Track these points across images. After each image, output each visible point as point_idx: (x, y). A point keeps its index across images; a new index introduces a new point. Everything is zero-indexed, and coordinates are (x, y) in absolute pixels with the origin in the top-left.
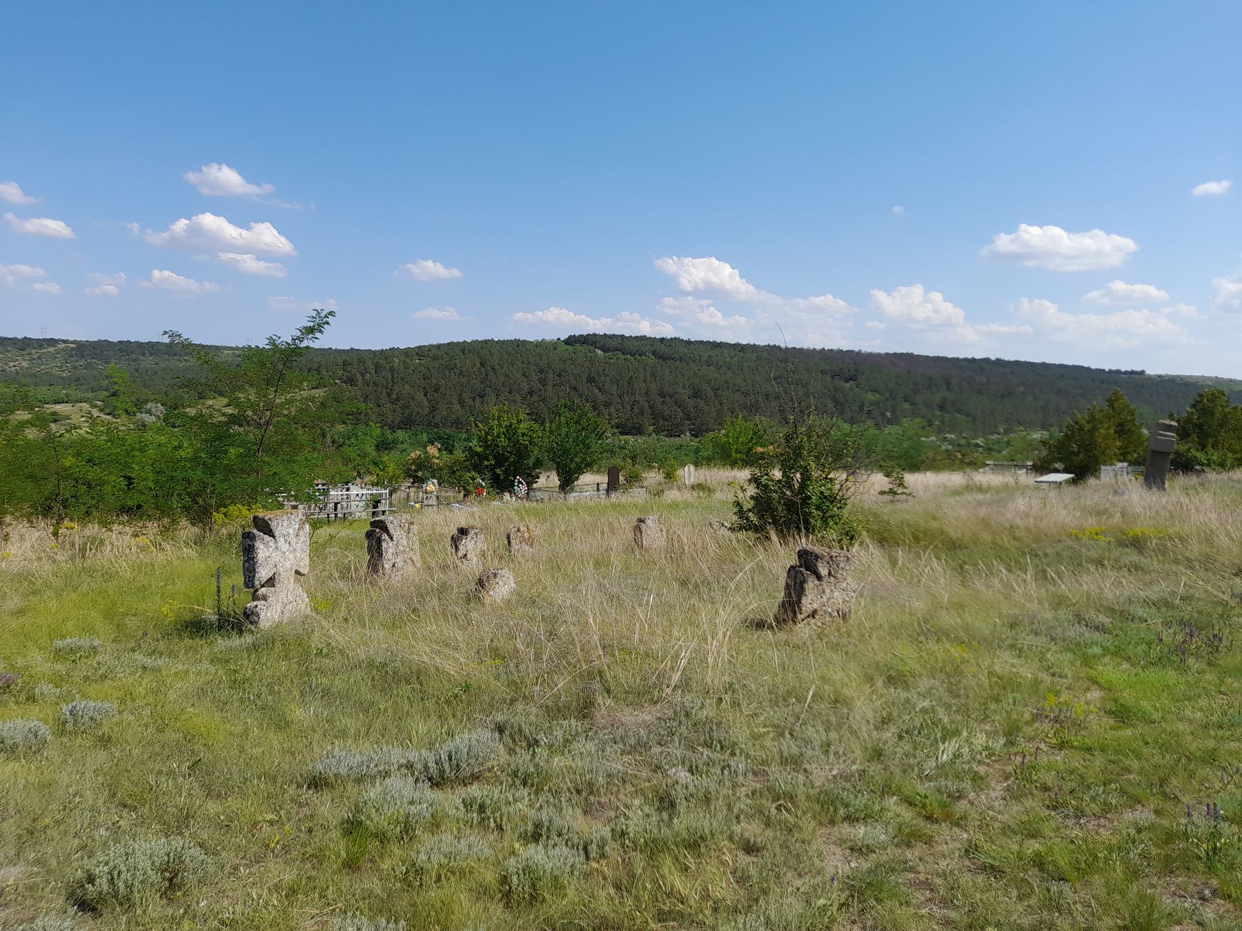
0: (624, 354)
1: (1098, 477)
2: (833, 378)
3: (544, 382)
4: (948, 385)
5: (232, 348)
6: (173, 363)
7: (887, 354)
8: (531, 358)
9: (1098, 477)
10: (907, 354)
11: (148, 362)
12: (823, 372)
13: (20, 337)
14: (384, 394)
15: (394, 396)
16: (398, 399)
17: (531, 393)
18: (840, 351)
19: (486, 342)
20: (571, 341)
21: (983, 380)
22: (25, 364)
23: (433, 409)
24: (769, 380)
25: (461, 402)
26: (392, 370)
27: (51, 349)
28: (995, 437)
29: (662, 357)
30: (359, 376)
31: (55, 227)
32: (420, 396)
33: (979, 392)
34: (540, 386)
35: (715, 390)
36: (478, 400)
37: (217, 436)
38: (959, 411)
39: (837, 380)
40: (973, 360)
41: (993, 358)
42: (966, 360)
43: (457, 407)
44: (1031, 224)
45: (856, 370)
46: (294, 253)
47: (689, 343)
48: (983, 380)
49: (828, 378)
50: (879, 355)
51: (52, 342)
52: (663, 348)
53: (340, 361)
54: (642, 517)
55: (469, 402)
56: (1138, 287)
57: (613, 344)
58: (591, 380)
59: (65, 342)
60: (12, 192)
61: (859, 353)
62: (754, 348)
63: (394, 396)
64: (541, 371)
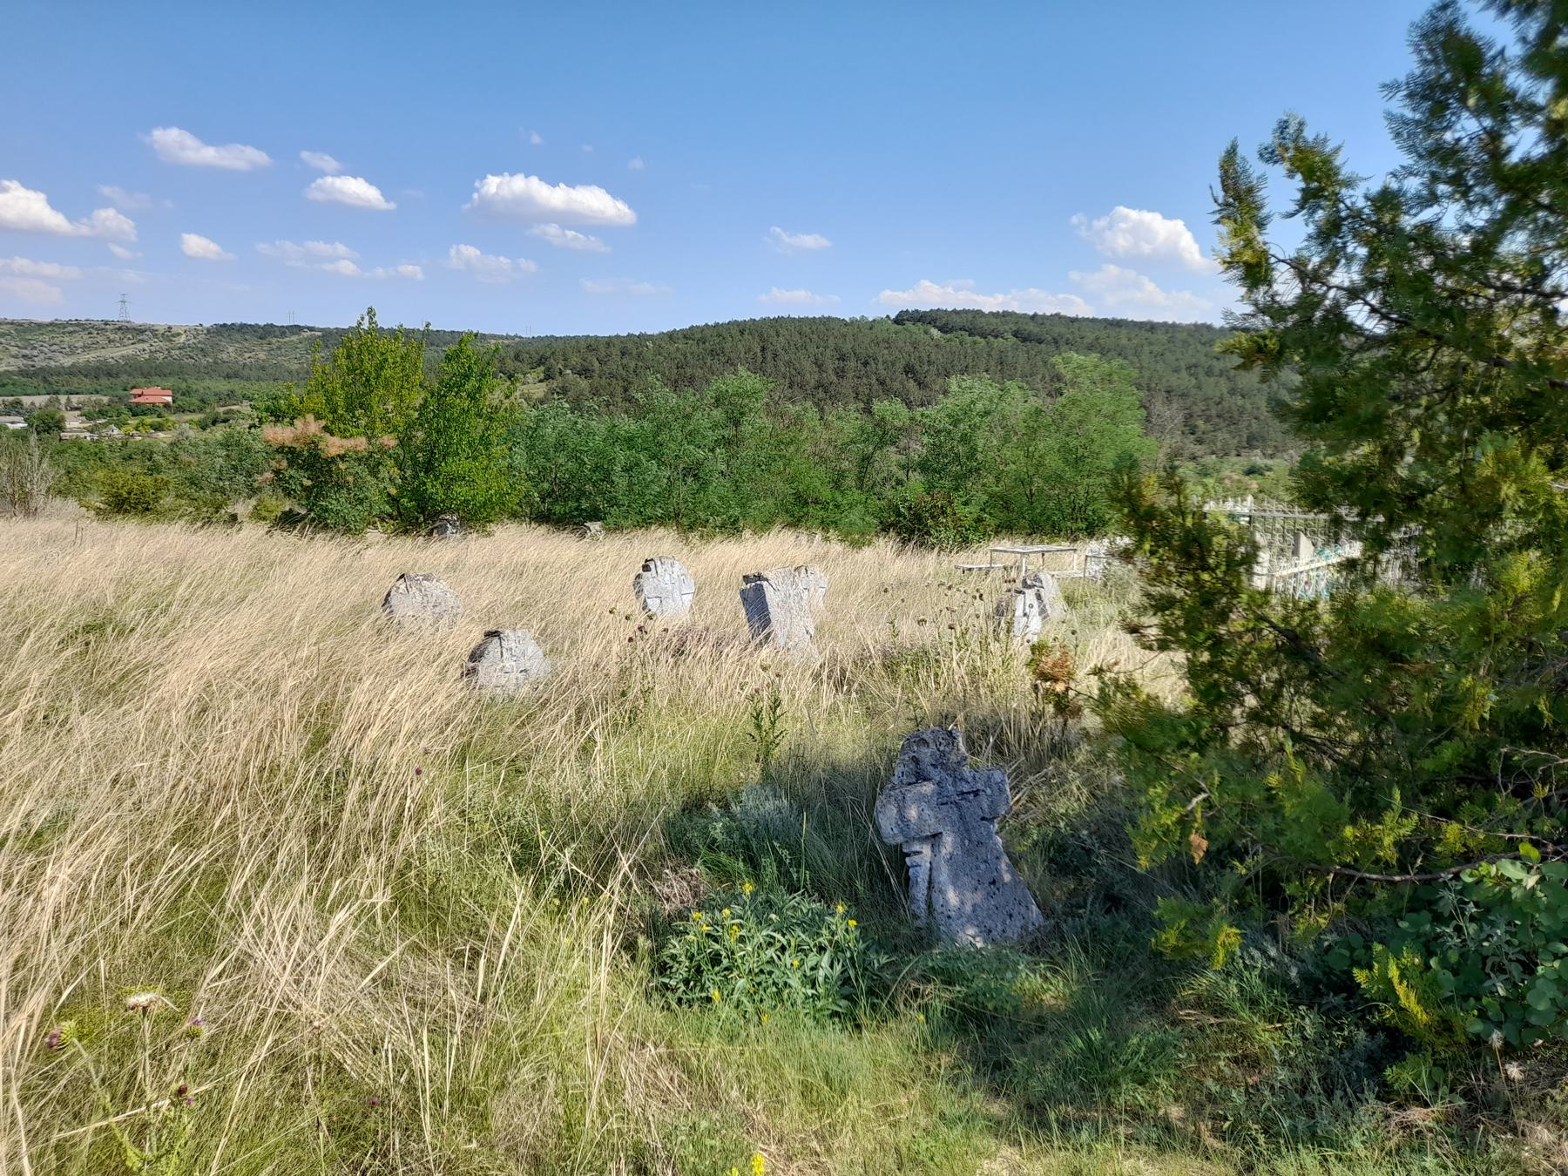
1: (900, 553)
3: (841, 374)
5: (501, 337)
8: (831, 342)
9: (900, 553)
13: (262, 323)
17: (819, 385)
22: (262, 356)
24: (1177, 370)
27: (294, 338)
29: (1023, 337)
44: (26, 185)
47: (1074, 320)
51: (297, 329)
52: (1032, 328)
53: (583, 345)
54: (491, 627)
57: (958, 320)
58: (909, 370)
59: (311, 329)
60: (24, 204)
64: (842, 358)
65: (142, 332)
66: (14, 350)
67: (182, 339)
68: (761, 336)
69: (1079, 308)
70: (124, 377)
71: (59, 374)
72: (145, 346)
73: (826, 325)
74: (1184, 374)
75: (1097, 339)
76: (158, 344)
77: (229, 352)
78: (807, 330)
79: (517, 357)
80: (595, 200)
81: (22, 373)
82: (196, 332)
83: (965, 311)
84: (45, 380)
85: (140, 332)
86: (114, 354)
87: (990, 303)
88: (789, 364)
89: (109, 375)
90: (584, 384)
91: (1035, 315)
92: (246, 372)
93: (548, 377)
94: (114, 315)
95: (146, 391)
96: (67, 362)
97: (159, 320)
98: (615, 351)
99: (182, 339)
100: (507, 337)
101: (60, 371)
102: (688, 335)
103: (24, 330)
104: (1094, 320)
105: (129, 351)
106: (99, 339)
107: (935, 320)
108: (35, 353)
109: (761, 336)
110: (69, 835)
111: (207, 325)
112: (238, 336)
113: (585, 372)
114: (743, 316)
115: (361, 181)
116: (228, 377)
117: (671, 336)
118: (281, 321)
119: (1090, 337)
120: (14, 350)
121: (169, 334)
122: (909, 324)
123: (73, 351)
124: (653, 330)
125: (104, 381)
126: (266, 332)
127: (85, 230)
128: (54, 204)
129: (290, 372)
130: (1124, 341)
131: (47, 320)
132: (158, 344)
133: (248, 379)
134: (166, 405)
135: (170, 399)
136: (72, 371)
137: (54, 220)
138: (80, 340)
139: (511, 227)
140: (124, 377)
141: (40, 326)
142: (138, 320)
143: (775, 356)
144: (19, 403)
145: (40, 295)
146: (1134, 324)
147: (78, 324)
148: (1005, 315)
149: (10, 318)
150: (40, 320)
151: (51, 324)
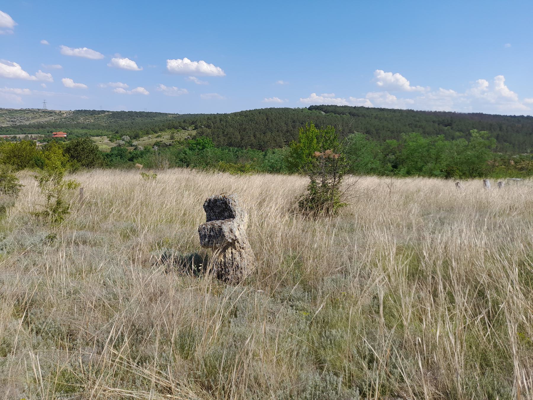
0: (335, 114)
2: (439, 124)
4: (501, 129)
5: (172, 114)
6: (149, 120)
7: (469, 114)
10: (480, 113)
11: (139, 120)
12: (434, 122)
13: (91, 110)
14: (221, 133)
15: (226, 133)
16: (227, 135)
17: (287, 131)
18: (445, 113)
19: (271, 109)
20: (311, 108)
21: (520, 125)
22: (92, 121)
23: (242, 139)
24: (405, 126)
25: (255, 136)
26: (226, 121)
27: (103, 115)
28: (525, 154)
29: (354, 115)
30: (212, 124)
31: (59, 67)
32: (237, 133)
33: (517, 132)
34: (292, 128)
35: (377, 130)
36: (263, 135)
37: (78, 143)
38: (505, 141)
39: (441, 126)
40: (515, 116)
41: (525, 115)
42: (511, 116)
43: (252, 138)
45: (451, 121)
46: (225, 75)
47: (368, 108)
48: (520, 125)
49: (436, 125)
50: (465, 114)
51: (103, 112)
52: (354, 111)
53: (206, 117)
55: (258, 135)
56: (77, 51)
59: (108, 112)
61: (454, 114)
62: (400, 111)
63: (226, 133)
65: (51, 113)
66: (8, 119)
67: (65, 115)
68: (266, 115)
69: (368, 104)
70: (48, 128)
71: (26, 127)
72: (53, 117)
73: (286, 111)
74: (407, 127)
75: (377, 115)
76: (57, 117)
77: (81, 120)
78: (281, 112)
79: (184, 122)
80: (206, 67)
81: (13, 127)
82: (69, 112)
83: (332, 106)
84: (21, 129)
85: (50, 113)
86: (43, 120)
87: (340, 102)
88: (277, 124)
89: (42, 127)
90: (209, 131)
91: (355, 107)
92: (88, 127)
93: (196, 128)
94: (41, 107)
95: (58, 133)
96: (28, 123)
97: (57, 109)
98: (218, 119)
99: (65, 115)
100: (174, 114)
101: (25, 126)
102: (241, 114)
103: (11, 112)
104: (374, 108)
105: (47, 119)
106: (37, 115)
107: (322, 109)
108: (15, 120)
109: (266, 115)
110: (522, 288)
111: (73, 110)
112: (84, 114)
113: (208, 127)
114: (259, 107)
115: (212, 65)
116: (82, 128)
117: (235, 114)
118: (97, 109)
119: (375, 114)
120: (8, 119)
121: (60, 113)
122: (314, 110)
123: (28, 119)
124: (229, 112)
125: (41, 129)
126: (93, 113)
127: (33, 78)
128: (23, 69)
129: (104, 127)
130: (386, 116)
131: (19, 109)
132: (57, 117)
133: (89, 129)
134: (65, 138)
135: (66, 136)
136: (30, 126)
137: (24, 74)
138: (30, 115)
139: (181, 77)
140: (48, 128)
141: (16, 111)
142: (49, 108)
143: (272, 121)
144: (16, 137)
145: (17, 100)
146: (389, 110)
147: (29, 110)
148: (346, 107)
149: (6, 108)
150: (16, 109)
151: (20, 110)
